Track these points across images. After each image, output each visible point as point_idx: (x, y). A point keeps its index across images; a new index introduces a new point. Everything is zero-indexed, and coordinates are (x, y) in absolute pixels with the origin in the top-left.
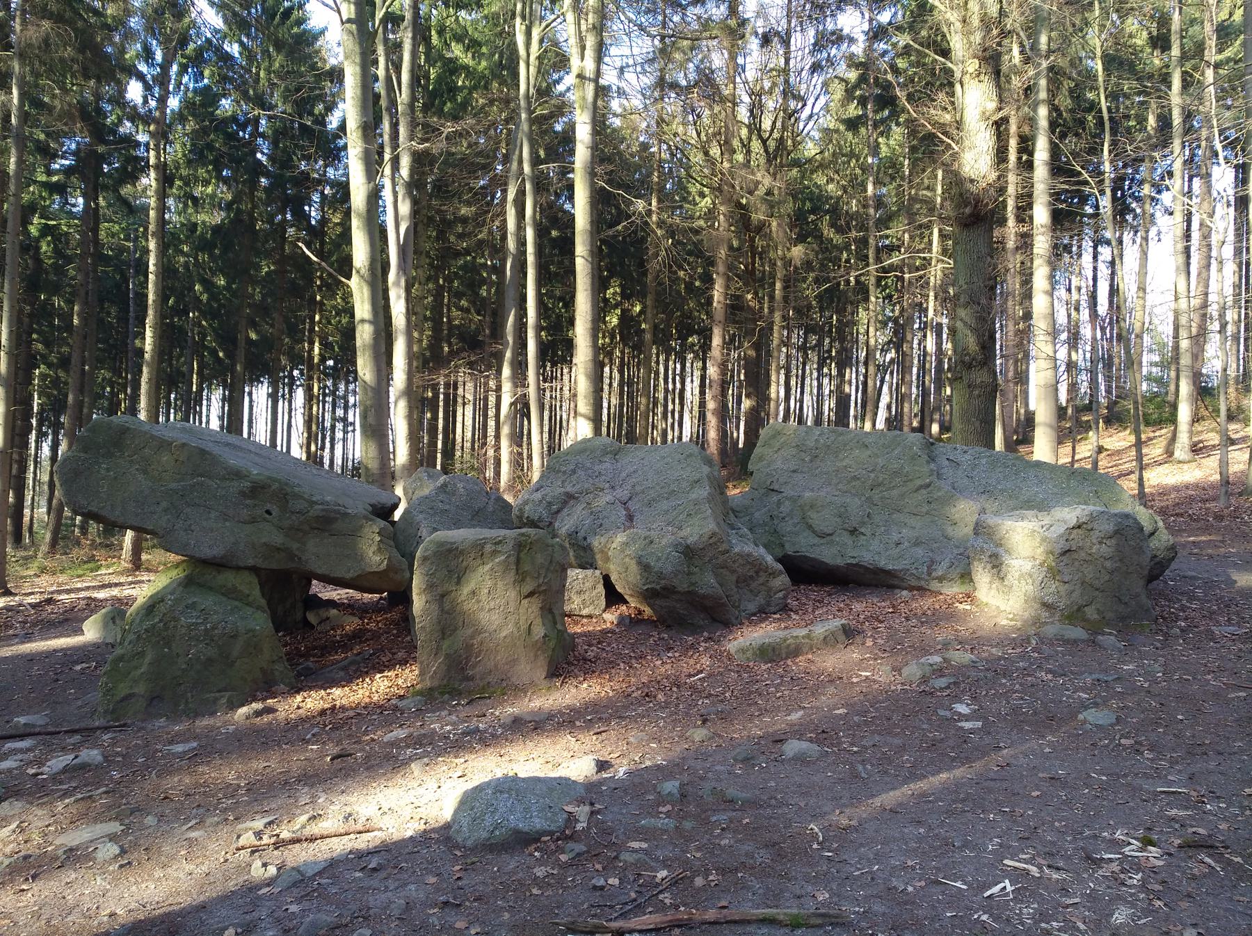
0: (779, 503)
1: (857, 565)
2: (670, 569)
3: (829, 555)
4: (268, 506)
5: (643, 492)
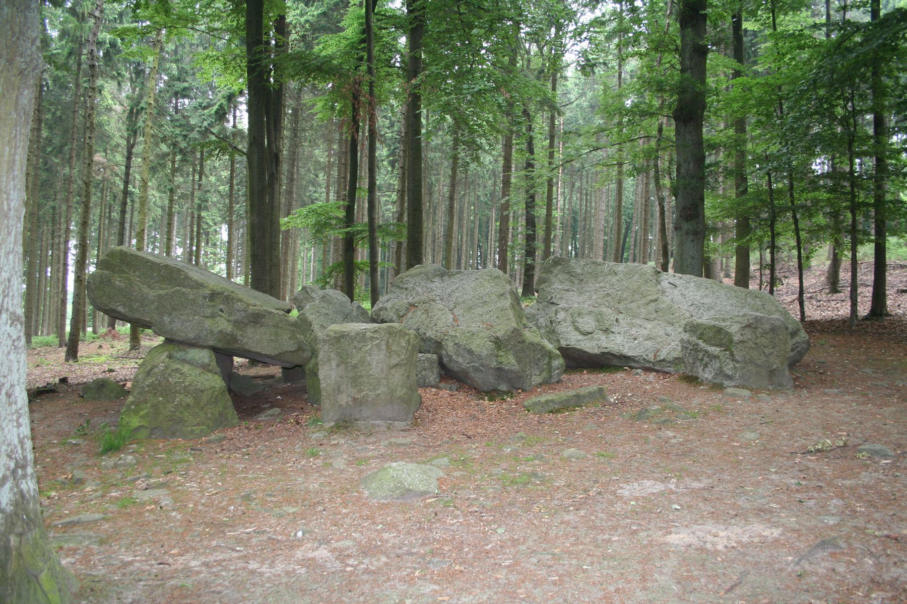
0: (556, 312)
1: (608, 353)
2: (485, 352)
3: (589, 346)
4: (222, 307)
5: (464, 302)
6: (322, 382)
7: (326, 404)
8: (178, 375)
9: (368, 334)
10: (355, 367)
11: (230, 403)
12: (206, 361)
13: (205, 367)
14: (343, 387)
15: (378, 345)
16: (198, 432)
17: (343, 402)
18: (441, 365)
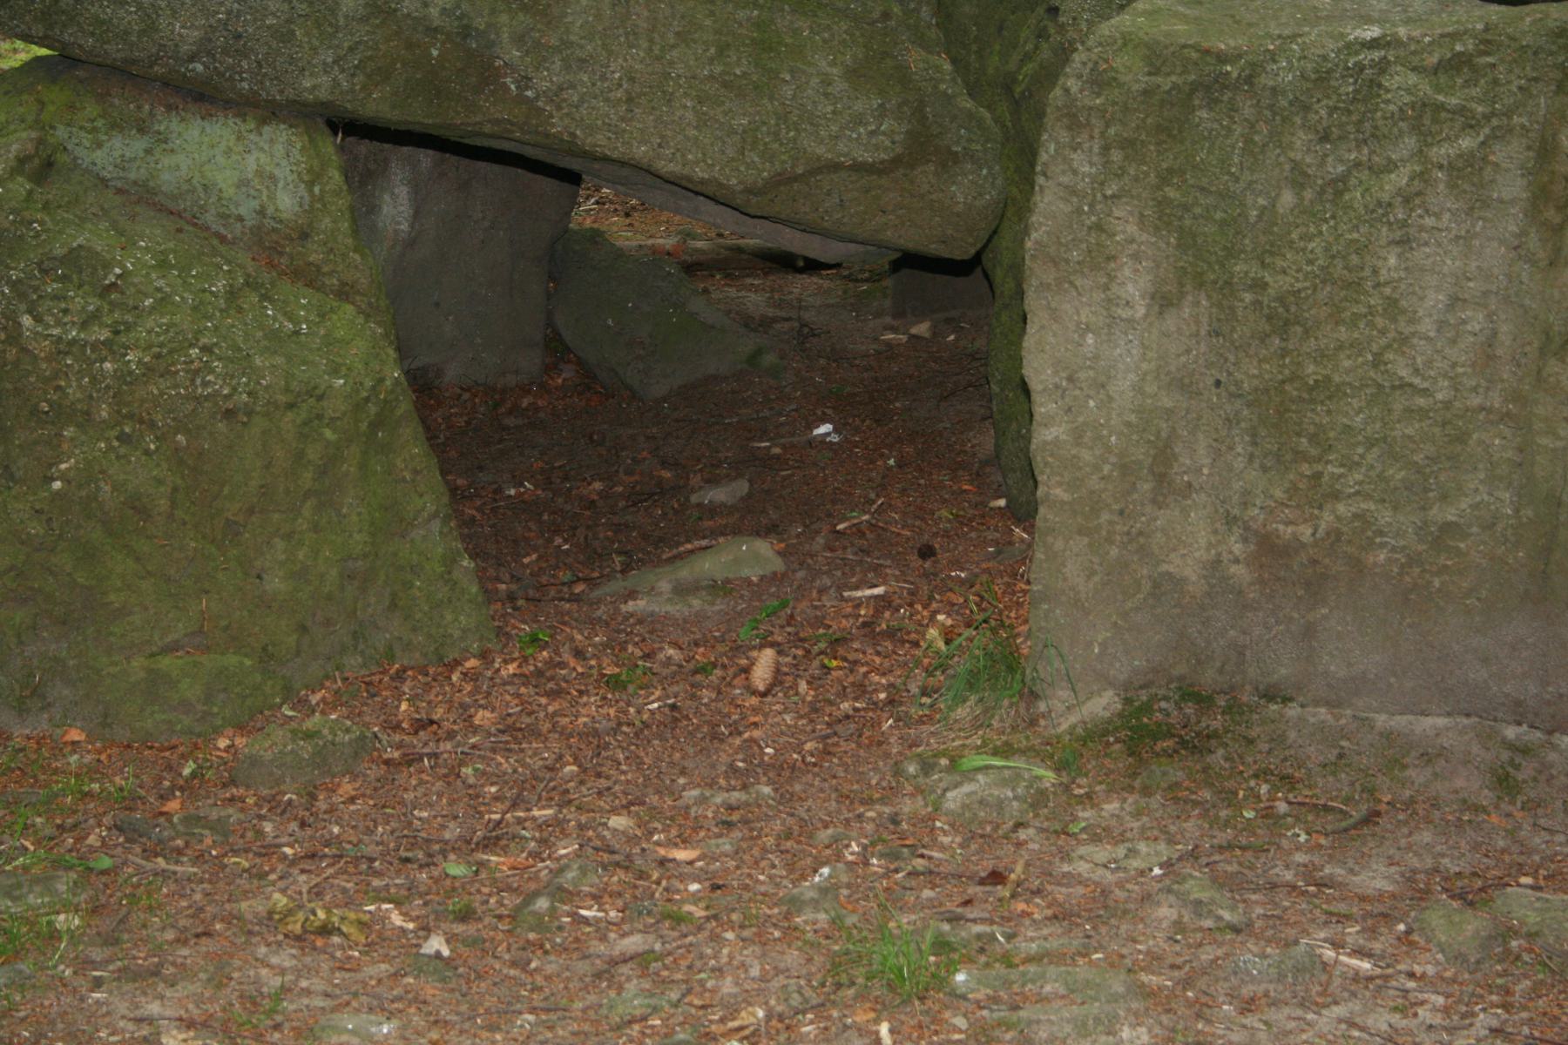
6: (1043, 407)
7: (1065, 560)
8: (81, 301)
9: (1402, 83)
10: (1283, 320)
11: (427, 499)
12: (287, 202)
13: (278, 252)
14: (1195, 458)
15: (1467, 170)
16: (190, 690)
17: (1187, 566)
18: (41, 110)
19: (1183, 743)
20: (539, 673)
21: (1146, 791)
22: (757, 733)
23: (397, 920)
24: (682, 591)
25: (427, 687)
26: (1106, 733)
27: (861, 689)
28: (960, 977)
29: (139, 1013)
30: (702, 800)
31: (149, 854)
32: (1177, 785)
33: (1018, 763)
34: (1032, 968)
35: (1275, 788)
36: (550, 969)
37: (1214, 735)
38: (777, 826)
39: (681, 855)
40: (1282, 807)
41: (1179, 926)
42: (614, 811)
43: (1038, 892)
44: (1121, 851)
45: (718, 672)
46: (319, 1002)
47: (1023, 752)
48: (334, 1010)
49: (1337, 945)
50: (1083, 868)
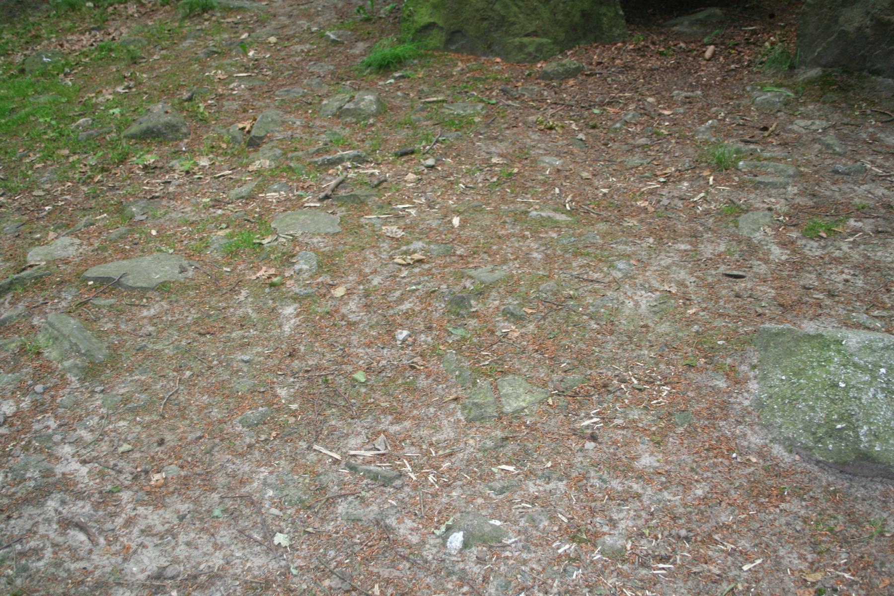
16: (531, 49)
19: (840, 87)
20: (639, 49)
21: (824, 103)
22: (702, 73)
23: (574, 126)
24: (692, 24)
25: (603, 51)
26: (814, 82)
27: (739, 61)
28: (741, 163)
29: (489, 151)
30: (678, 95)
31: (508, 99)
32: (835, 102)
33: (783, 90)
34: (766, 162)
35: (868, 105)
36: (614, 147)
37: (851, 86)
38: (700, 105)
39: (666, 112)
40: (869, 112)
41: (820, 151)
42: (650, 96)
43: (778, 135)
44: (810, 122)
45: (695, 52)
46: (541, 152)
47: (785, 86)
48: (545, 155)
49: (872, 162)
50: (795, 127)
